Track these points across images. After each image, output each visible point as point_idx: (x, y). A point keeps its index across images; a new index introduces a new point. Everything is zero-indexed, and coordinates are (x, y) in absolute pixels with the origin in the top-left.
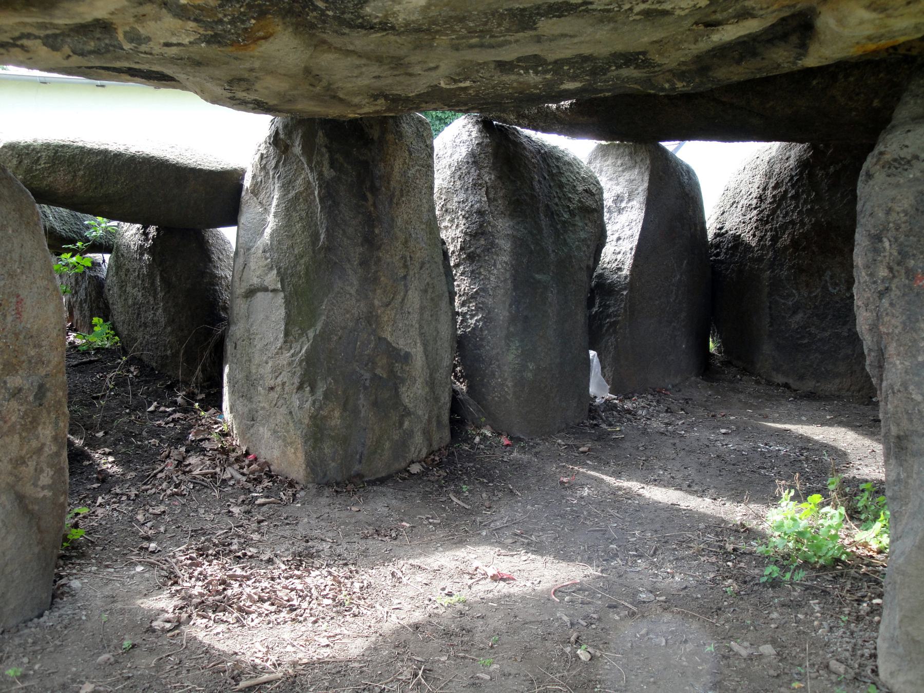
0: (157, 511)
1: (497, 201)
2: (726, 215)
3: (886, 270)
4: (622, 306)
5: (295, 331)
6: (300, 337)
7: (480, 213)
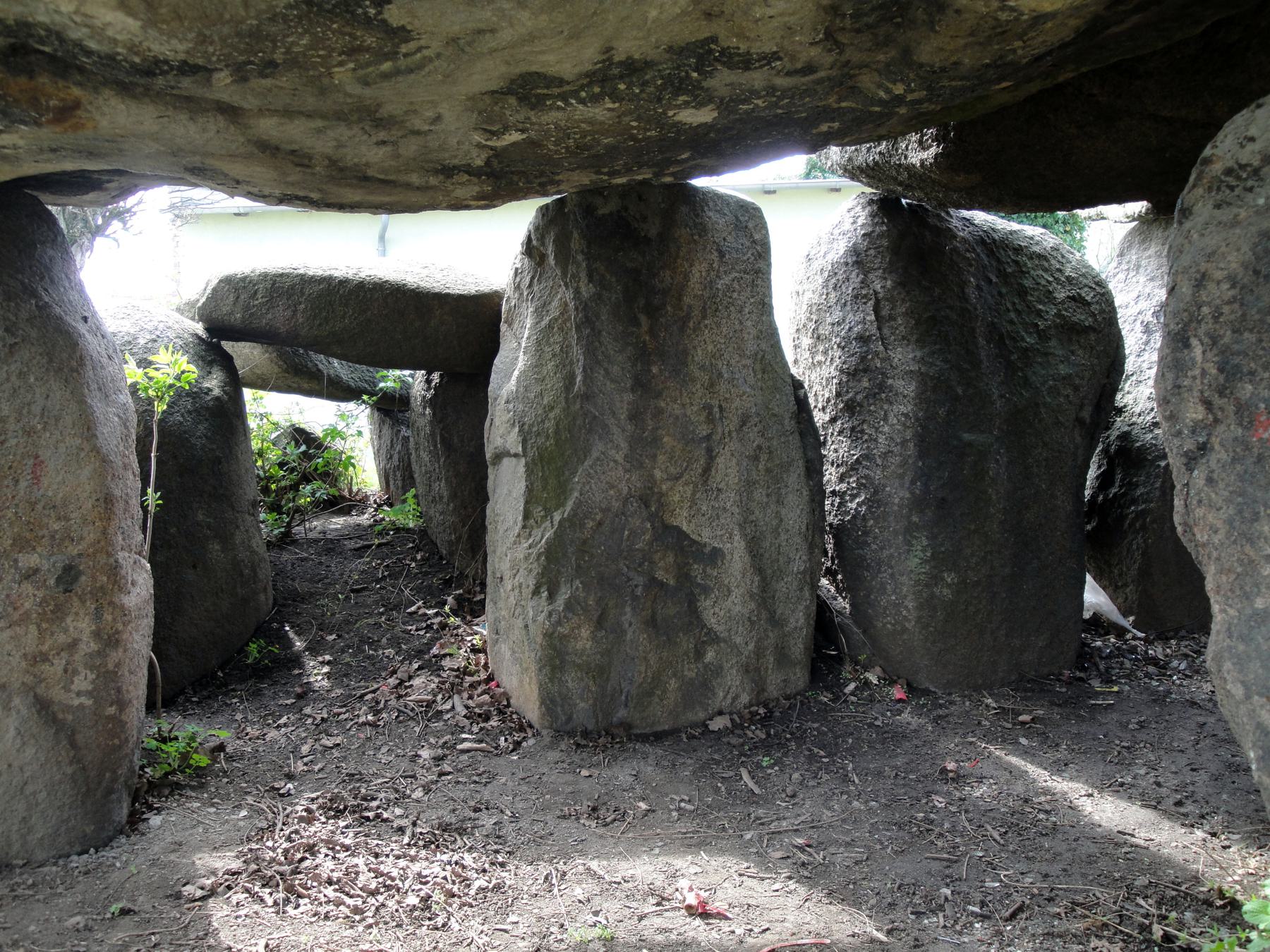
0: (329, 744)
1: (895, 320)
3: (1201, 408)
4: (1158, 485)
5: (538, 511)
6: (542, 522)
7: (863, 339)
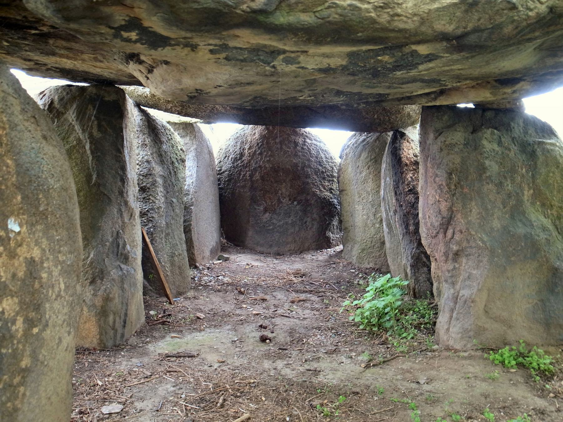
2: (222, 163)
